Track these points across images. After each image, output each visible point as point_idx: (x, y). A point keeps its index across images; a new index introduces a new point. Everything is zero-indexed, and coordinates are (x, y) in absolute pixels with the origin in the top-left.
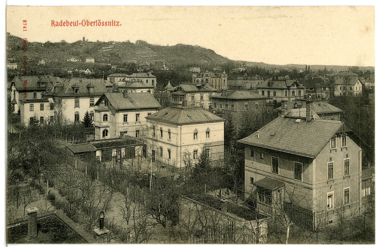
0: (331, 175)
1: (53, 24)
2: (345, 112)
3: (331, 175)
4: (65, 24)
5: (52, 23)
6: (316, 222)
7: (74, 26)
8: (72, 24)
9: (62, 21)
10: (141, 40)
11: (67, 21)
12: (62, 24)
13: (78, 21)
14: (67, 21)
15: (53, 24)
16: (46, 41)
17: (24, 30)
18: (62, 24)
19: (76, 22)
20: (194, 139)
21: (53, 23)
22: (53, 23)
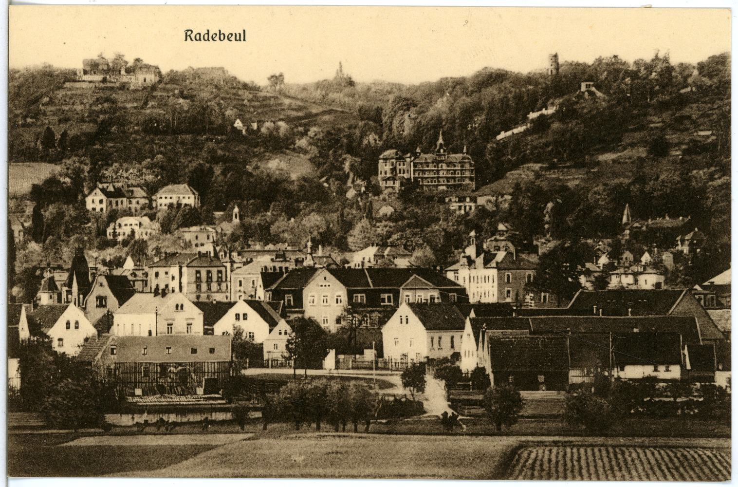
0: (407, 319)
1: (188, 38)
2: (704, 250)
3: (407, 319)
4: (217, 38)
5: (186, 36)
6: (266, 356)
7: (236, 40)
8: (233, 38)
9: (208, 31)
10: (235, 78)
11: (220, 31)
12: (208, 37)
13: (244, 31)
14: (220, 31)
15: (188, 38)
16: (329, 74)
17: (244, 40)
18: (208, 37)
19: (240, 34)
20: (401, 323)
21: (188, 34)
22: (188, 34)
